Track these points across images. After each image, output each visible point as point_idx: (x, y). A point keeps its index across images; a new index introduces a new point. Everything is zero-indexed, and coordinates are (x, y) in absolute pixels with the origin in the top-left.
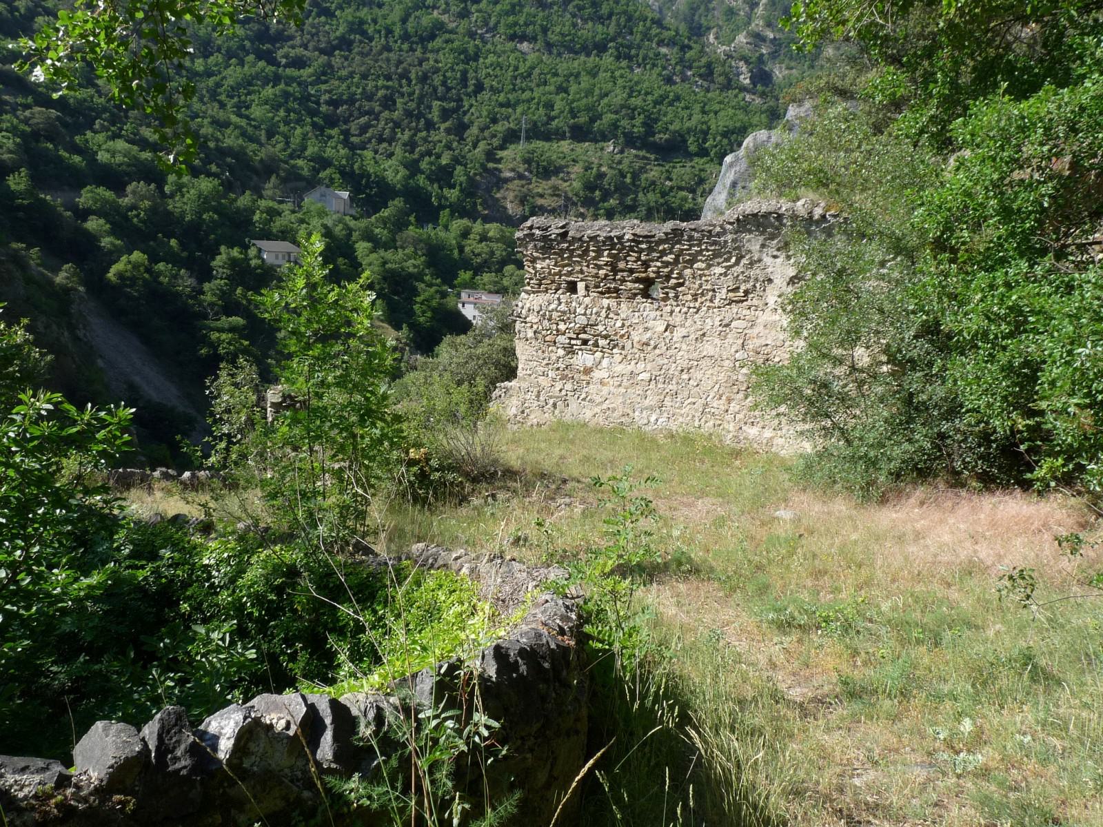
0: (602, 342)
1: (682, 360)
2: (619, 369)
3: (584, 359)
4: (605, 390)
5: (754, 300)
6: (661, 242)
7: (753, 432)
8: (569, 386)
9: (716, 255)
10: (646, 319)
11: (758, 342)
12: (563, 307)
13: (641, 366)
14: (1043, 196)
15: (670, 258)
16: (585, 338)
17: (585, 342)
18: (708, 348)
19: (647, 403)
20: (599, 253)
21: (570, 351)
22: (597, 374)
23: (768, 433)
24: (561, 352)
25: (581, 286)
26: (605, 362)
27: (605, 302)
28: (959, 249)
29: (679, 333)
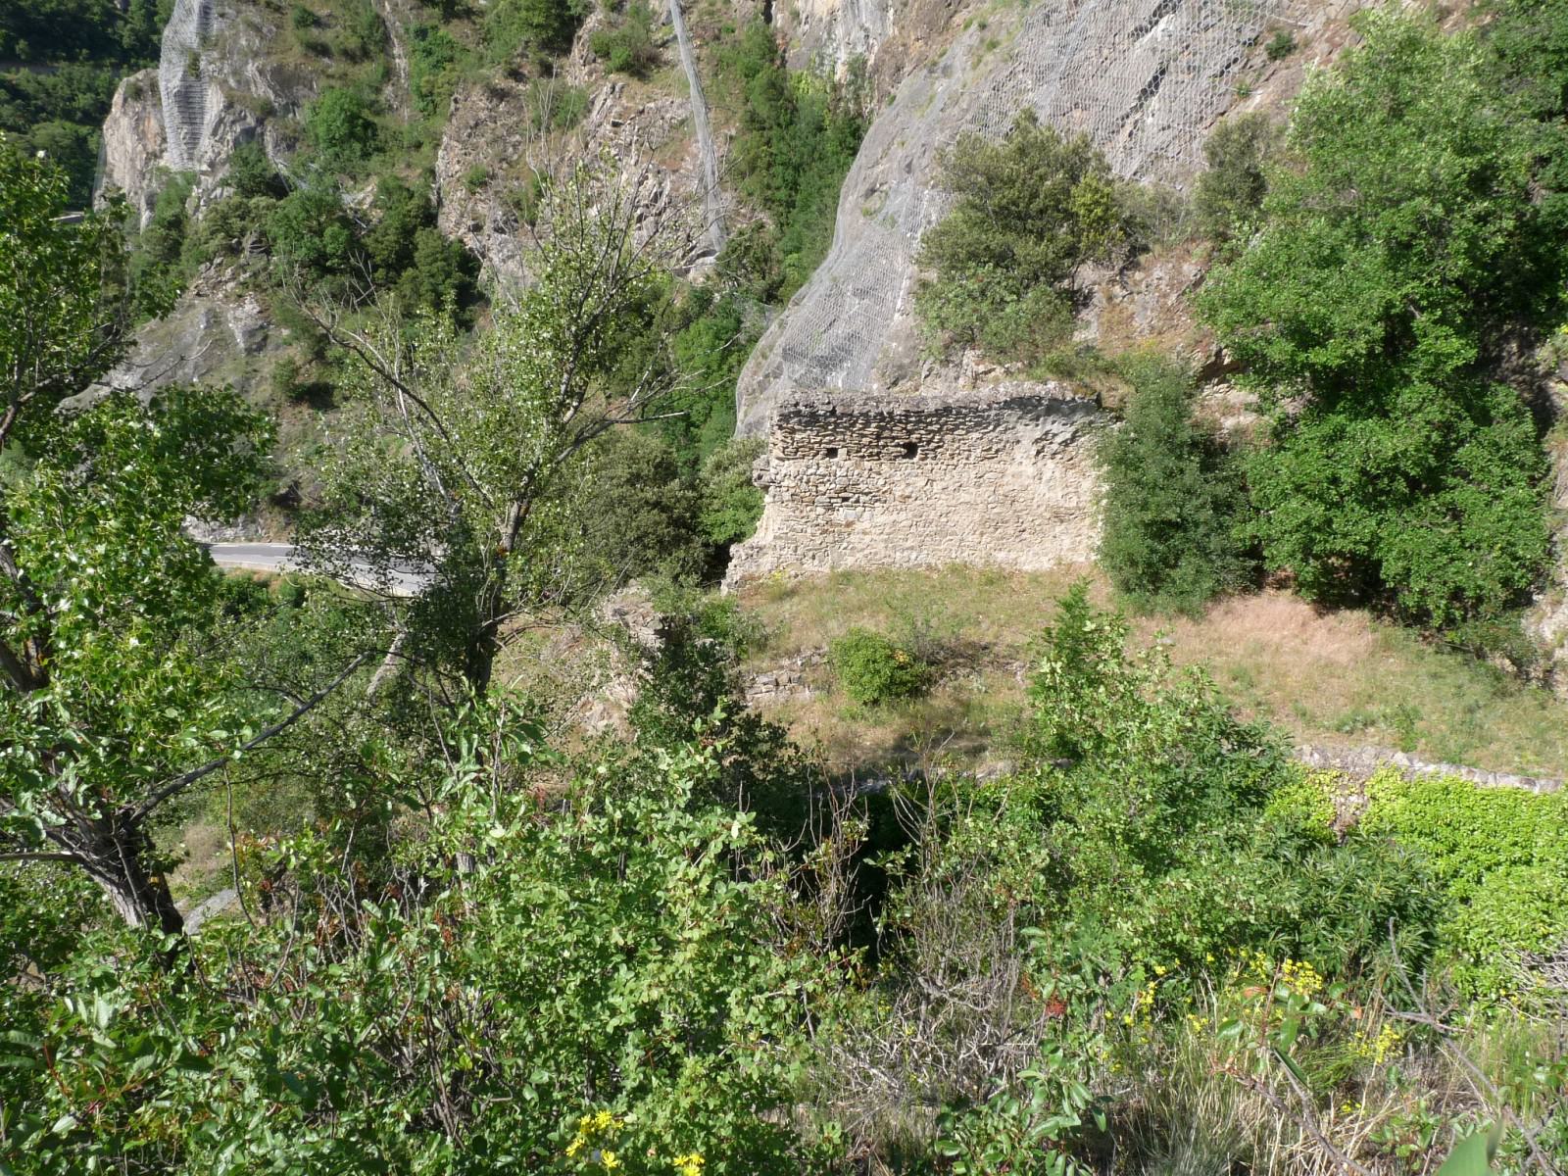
0: (863, 498)
1: (942, 505)
2: (881, 519)
3: (842, 514)
4: (867, 538)
5: (1002, 456)
6: (930, 415)
7: (1001, 556)
8: (830, 539)
9: (977, 424)
10: (905, 476)
11: (1007, 488)
12: (822, 471)
13: (903, 516)
14: (642, 1091)
15: (935, 427)
16: (845, 495)
17: (845, 499)
18: (964, 497)
19: (909, 544)
20: (867, 425)
21: (830, 508)
22: (858, 527)
23: (1013, 555)
24: (820, 510)
25: (842, 452)
26: (867, 515)
27: (867, 464)
28: (99, 426)
29: (937, 487)
